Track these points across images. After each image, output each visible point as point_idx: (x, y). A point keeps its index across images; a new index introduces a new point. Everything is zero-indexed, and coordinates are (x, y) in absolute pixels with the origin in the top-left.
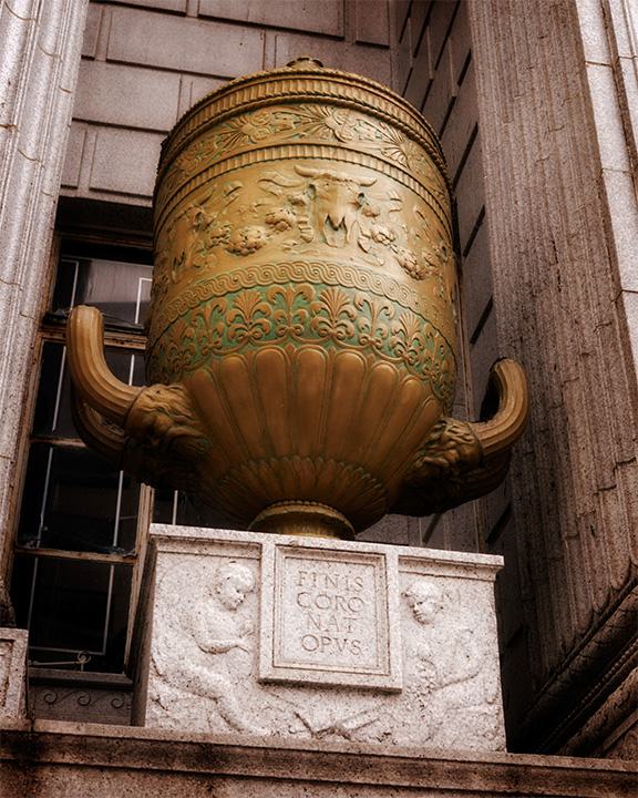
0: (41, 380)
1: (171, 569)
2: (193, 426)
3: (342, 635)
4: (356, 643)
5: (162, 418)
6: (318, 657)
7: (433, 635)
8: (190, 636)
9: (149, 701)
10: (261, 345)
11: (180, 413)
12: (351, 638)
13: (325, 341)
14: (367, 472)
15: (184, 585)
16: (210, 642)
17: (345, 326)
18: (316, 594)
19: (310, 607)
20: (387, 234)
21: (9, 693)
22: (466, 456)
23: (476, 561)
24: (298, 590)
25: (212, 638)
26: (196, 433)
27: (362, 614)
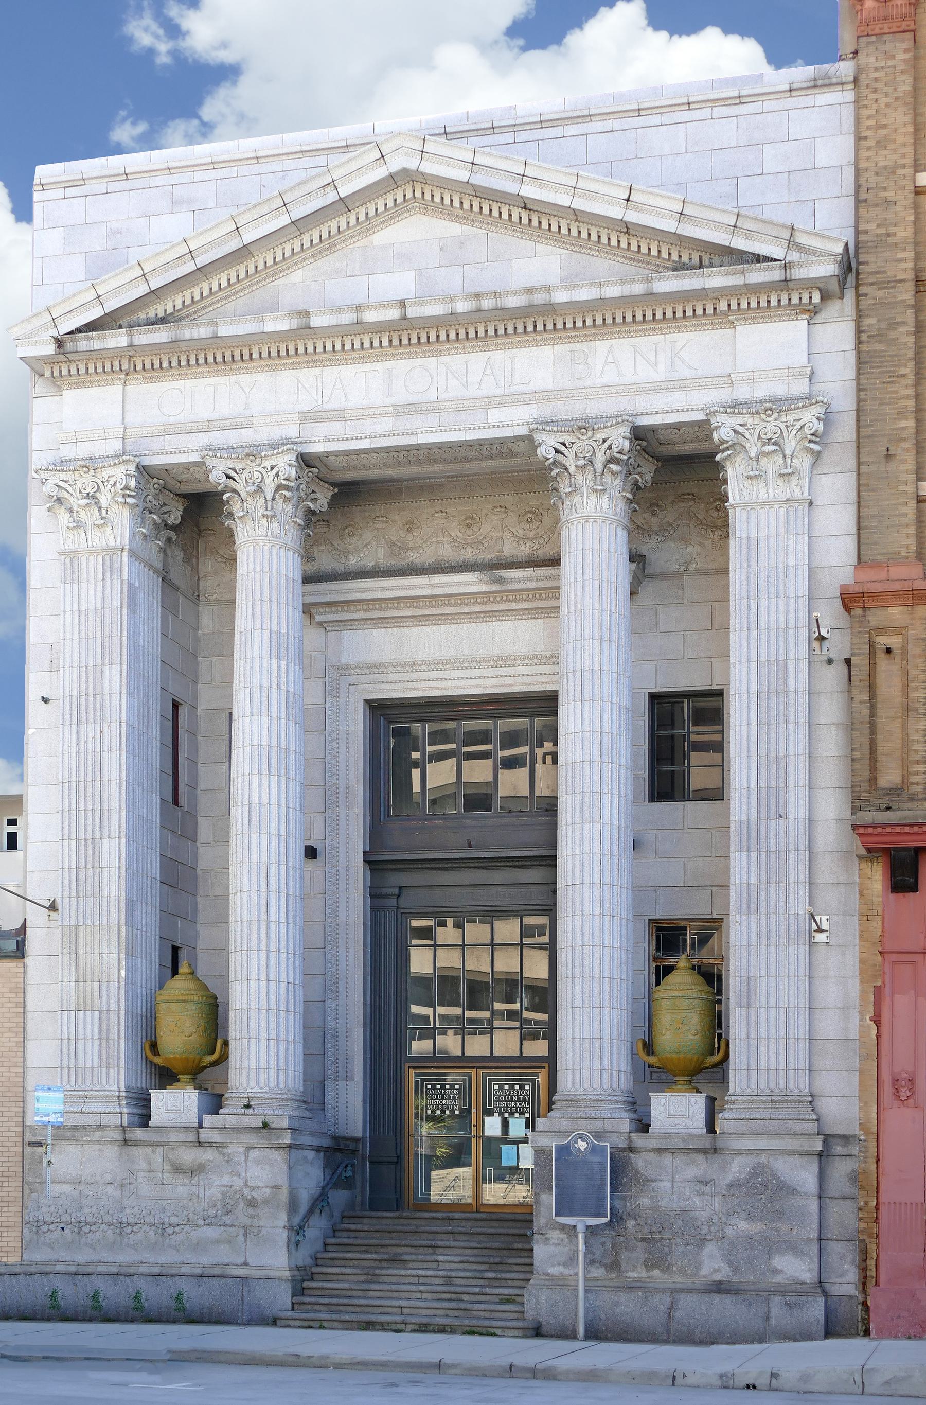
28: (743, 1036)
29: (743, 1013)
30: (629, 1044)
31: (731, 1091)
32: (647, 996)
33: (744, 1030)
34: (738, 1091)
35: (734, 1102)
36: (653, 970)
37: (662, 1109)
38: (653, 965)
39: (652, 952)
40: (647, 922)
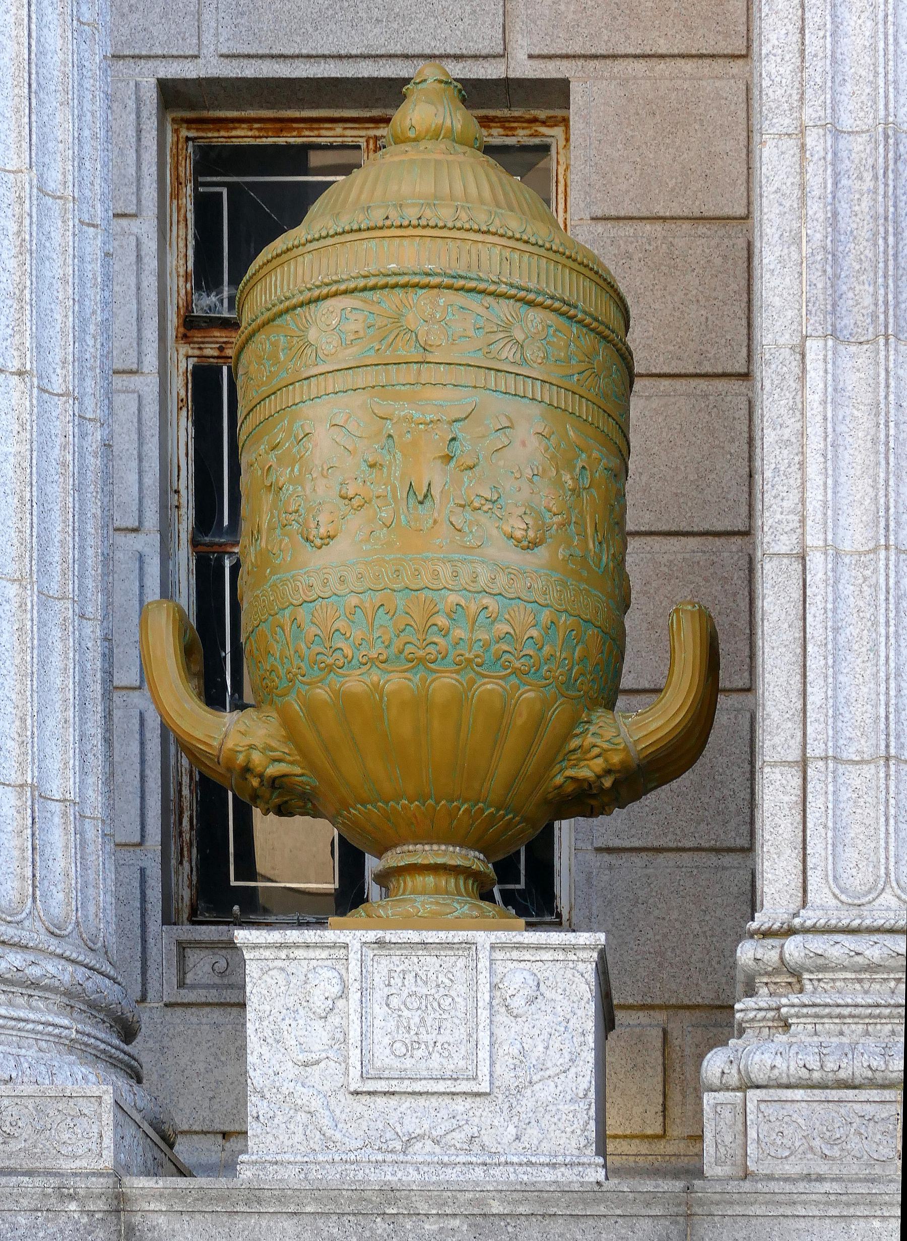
0: (197, 438)
1: (260, 978)
2: (292, 763)
3: (430, 1038)
4: (446, 1046)
5: (257, 758)
6: (408, 1063)
7: (526, 1030)
8: (283, 1050)
9: (250, 1119)
10: (345, 676)
11: (275, 750)
12: (441, 1039)
13: (413, 667)
14: (489, 807)
15: (274, 995)
16: (302, 1057)
17: (435, 643)
18: (405, 994)
19: (400, 1010)
20: (488, 495)
21: (104, 1146)
22: (614, 765)
23: (573, 942)
24: (387, 991)
25: (302, 1051)
26: (297, 770)
27: (453, 1013)
28: (855, 535)
29: (851, 380)
30: (92, 631)
31: (775, 905)
32: (152, 519)
33: (858, 491)
34: (824, 905)
35: (794, 975)
36: (179, 386)
37: (319, 1037)
38: (183, 361)
39: (179, 287)
40: (151, 95)
